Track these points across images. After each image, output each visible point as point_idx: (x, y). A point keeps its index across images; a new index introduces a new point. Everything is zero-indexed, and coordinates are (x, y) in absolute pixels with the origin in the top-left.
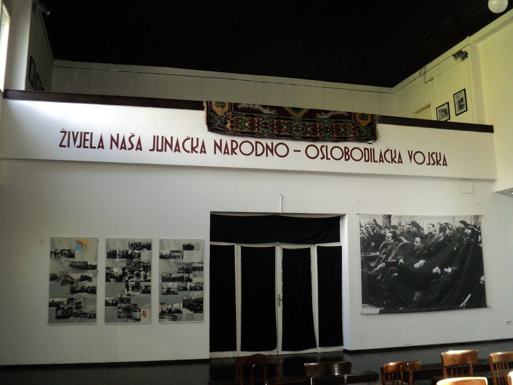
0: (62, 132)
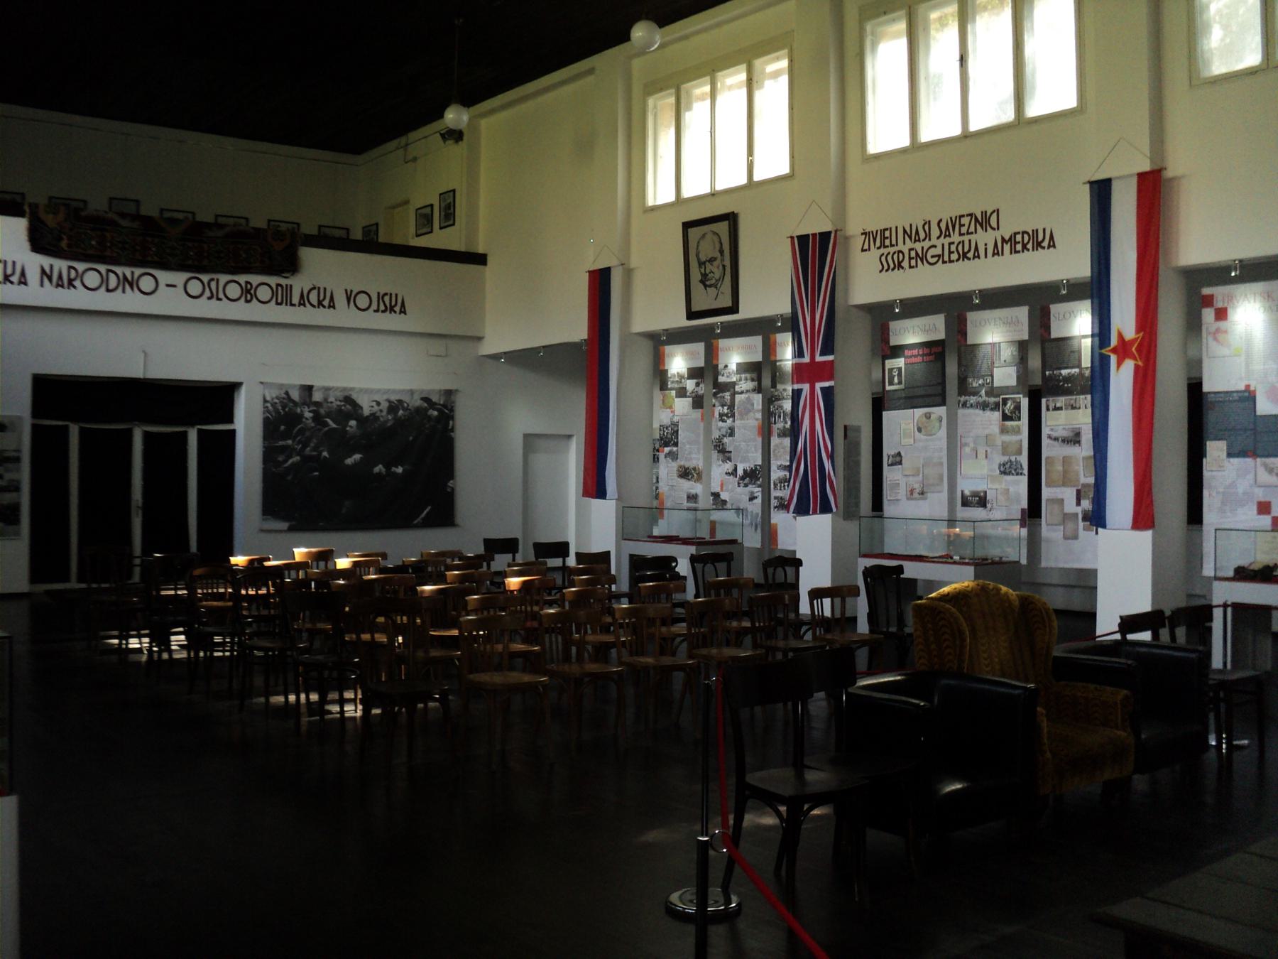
0: (862, 234)
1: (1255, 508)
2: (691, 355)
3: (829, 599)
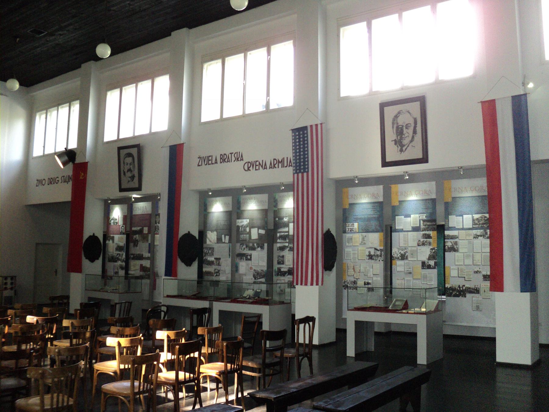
0: (198, 158)
1: (497, 294)
2: (260, 202)
3: (306, 343)
